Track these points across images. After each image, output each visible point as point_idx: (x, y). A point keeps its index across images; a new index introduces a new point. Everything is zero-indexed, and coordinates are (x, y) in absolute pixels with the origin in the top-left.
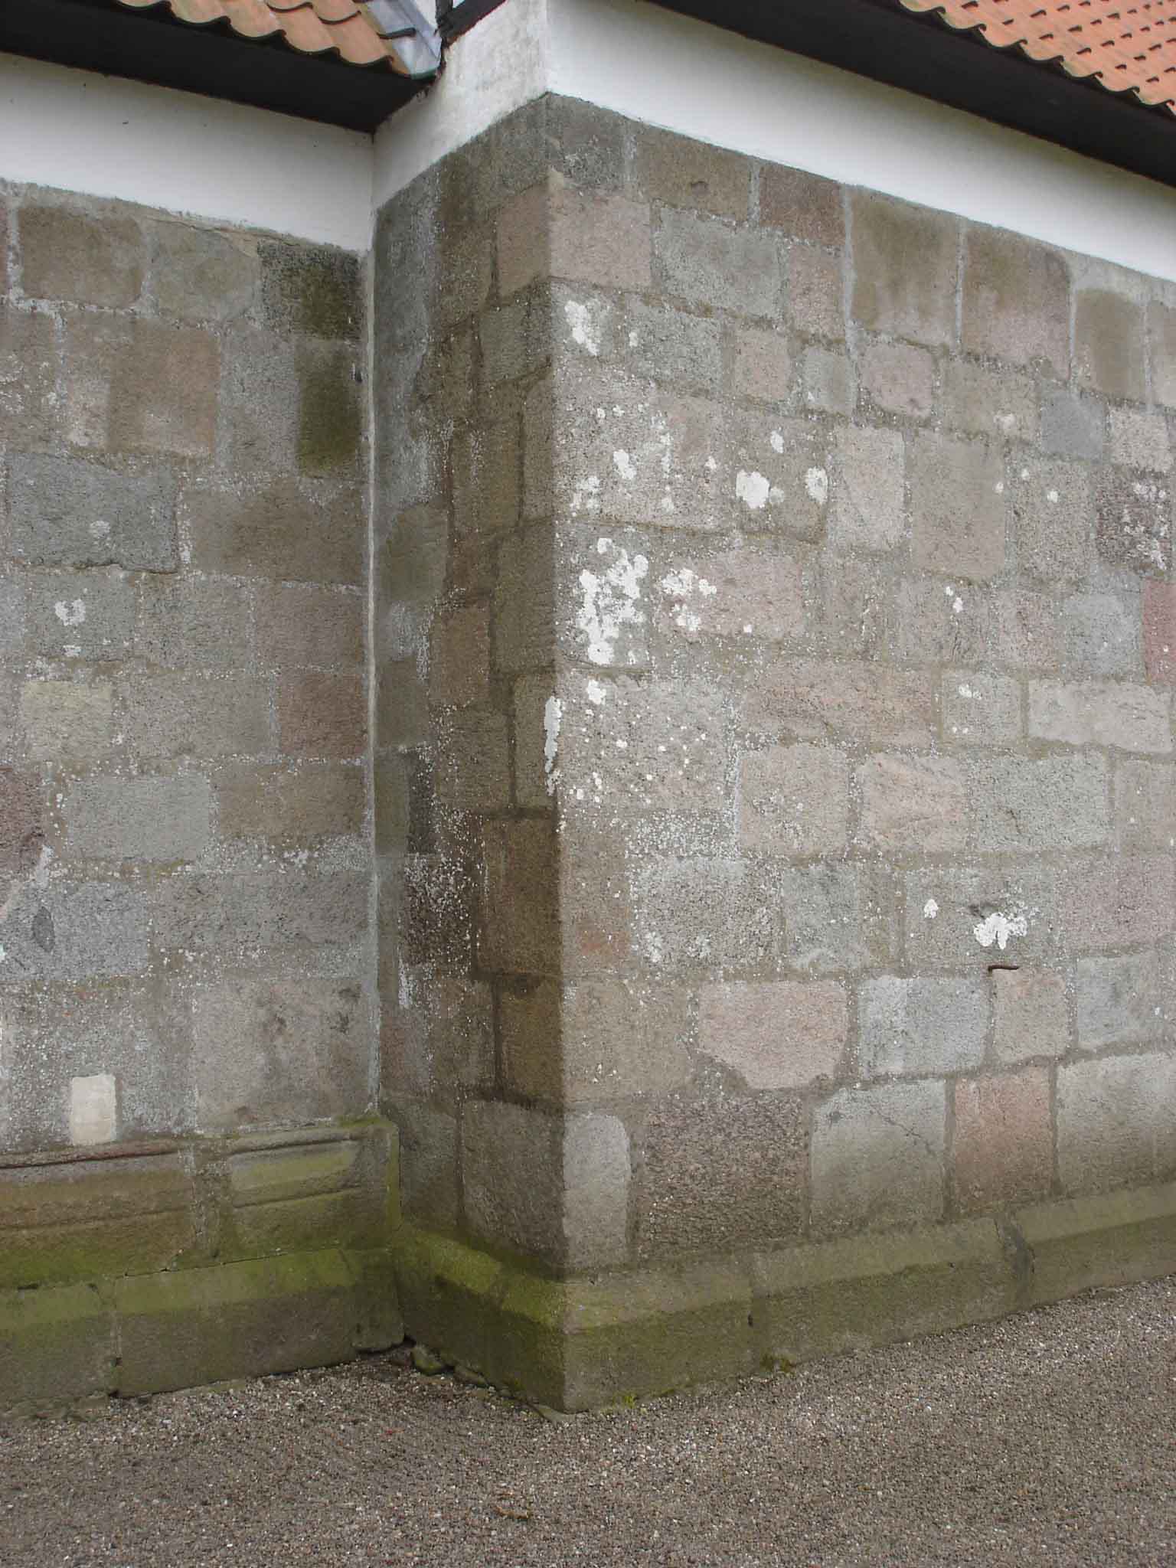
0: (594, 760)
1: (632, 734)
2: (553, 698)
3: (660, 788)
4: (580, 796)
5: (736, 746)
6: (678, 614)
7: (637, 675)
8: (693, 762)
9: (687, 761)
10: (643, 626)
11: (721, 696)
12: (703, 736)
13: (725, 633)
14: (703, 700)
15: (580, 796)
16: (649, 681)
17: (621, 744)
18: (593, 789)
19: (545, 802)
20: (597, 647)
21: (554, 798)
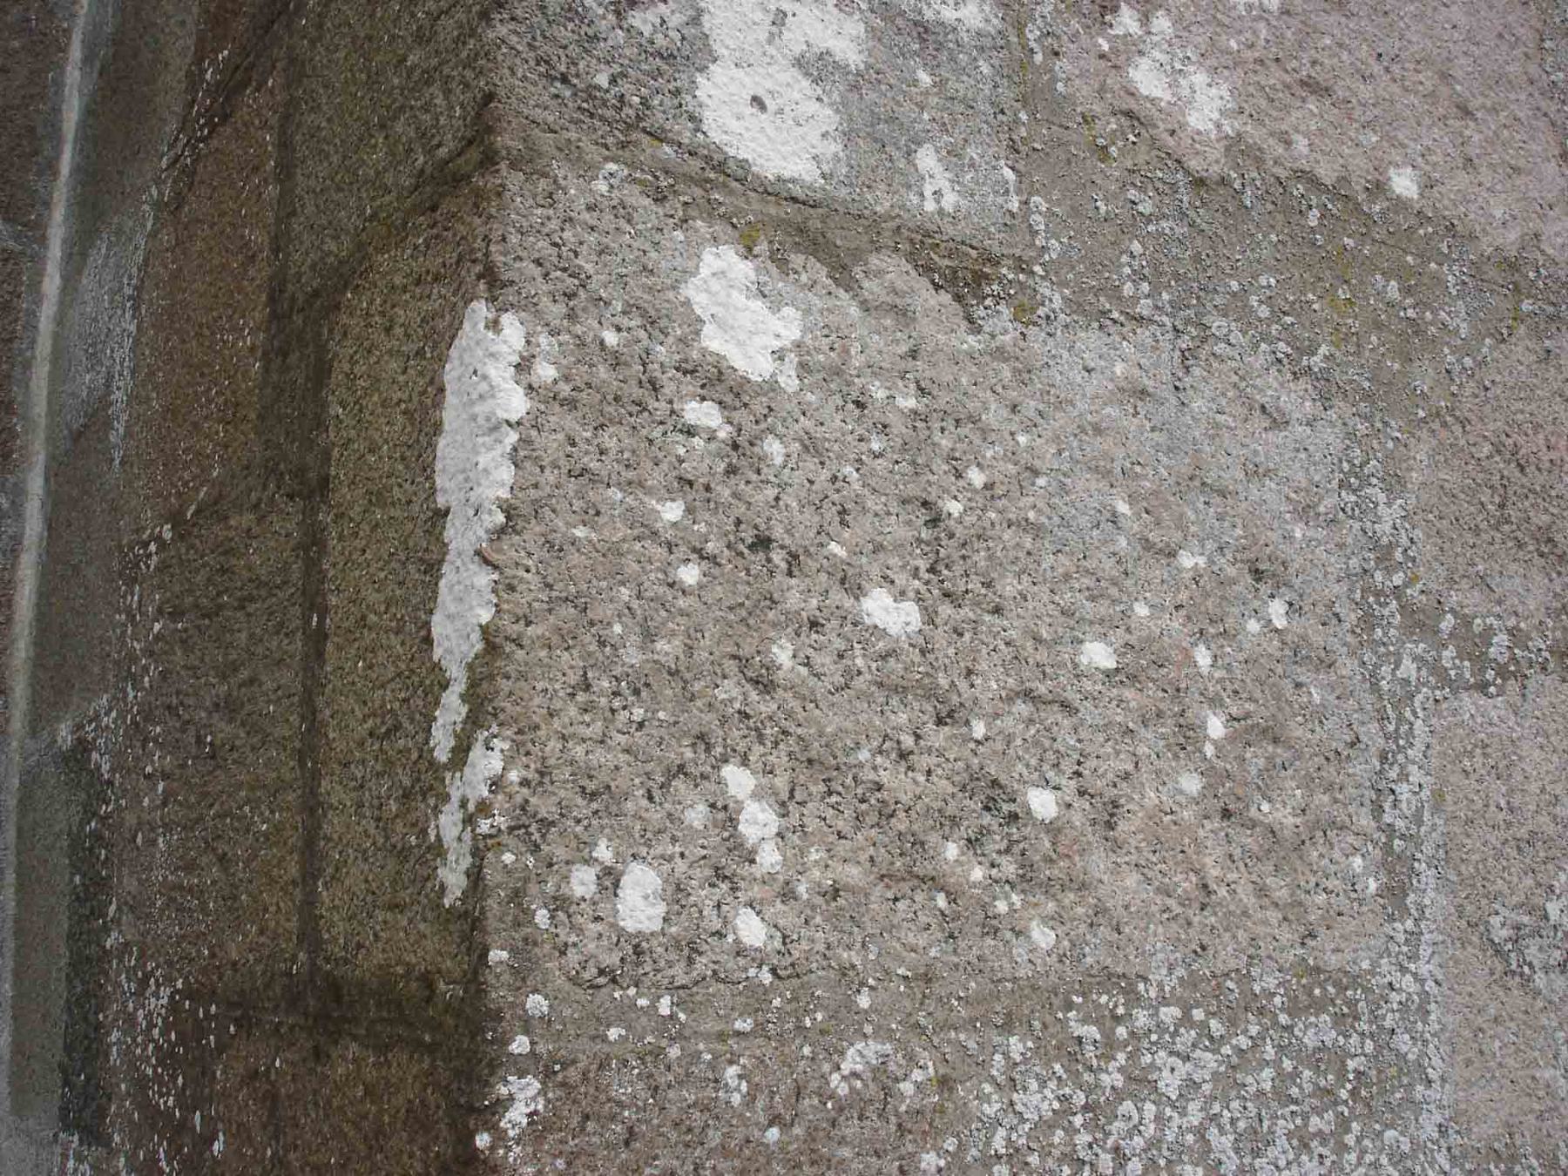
0: (730, 690)
1: (943, 564)
2: (480, 310)
3: (1098, 863)
4: (640, 904)
5: (1408, 668)
6: (1132, 48)
7: (967, 275)
8: (1245, 732)
9: (1216, 727)
10: (984, 44)
11: (1331, 437)
12: (1277, 611)
13: (1326, 173)
14: (1268, 445)
15: (640, 904)
16: (1025, 313)
17: (890, 613)
18: (728, 862)
19: (430, 948)
20: (751, 83)
21: (468, 925)
